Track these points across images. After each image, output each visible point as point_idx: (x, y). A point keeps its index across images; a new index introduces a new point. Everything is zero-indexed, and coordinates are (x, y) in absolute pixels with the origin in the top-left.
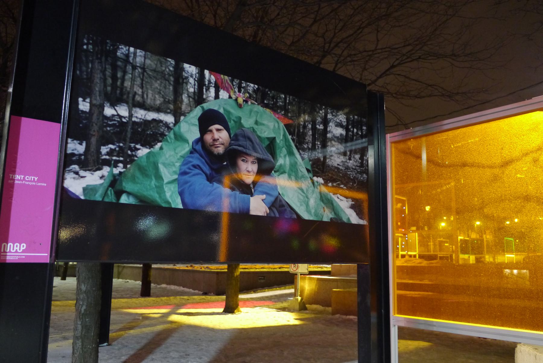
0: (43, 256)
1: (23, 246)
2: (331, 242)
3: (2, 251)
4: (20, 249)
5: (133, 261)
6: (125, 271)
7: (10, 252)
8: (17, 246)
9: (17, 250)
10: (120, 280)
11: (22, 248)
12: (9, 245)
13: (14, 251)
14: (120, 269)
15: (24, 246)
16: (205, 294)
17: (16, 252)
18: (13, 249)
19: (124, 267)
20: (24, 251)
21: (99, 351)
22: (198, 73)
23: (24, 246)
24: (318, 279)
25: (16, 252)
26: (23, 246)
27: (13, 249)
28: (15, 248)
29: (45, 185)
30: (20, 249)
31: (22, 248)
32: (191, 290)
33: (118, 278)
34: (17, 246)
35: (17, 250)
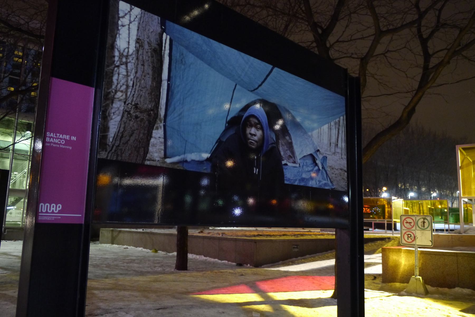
0: (77, 217)
1: (59, 207)
2: (306, 204)
3: (40, 211)
4: (56, 210)
5: (269, 219)
6: (121, 235)
7: (42, 212)
8: (53, 207)
9: (53, 210)
10: (115, 246)
11: (58, 209)
12: (41, 204)
13: (51, 211)
14: (115, 234)
15: (60, 207)
16: (240, 265)
17: (53, 212)
18: (50, 210)
19: (120, 231)
20: (60, 212)
21: (365, 297)
22: (119, 18)
23: (60, 207)
24: (422, 252)
25: (53, 212)
26: (59, 207)
27: (50, 210)
28: (52, 209)
29: (71, 148)
30: (56, 210)
31: (58, 209)
32: (216, 260)
33: (113, 243)
34: (53, 207)
35: (53, 210)
